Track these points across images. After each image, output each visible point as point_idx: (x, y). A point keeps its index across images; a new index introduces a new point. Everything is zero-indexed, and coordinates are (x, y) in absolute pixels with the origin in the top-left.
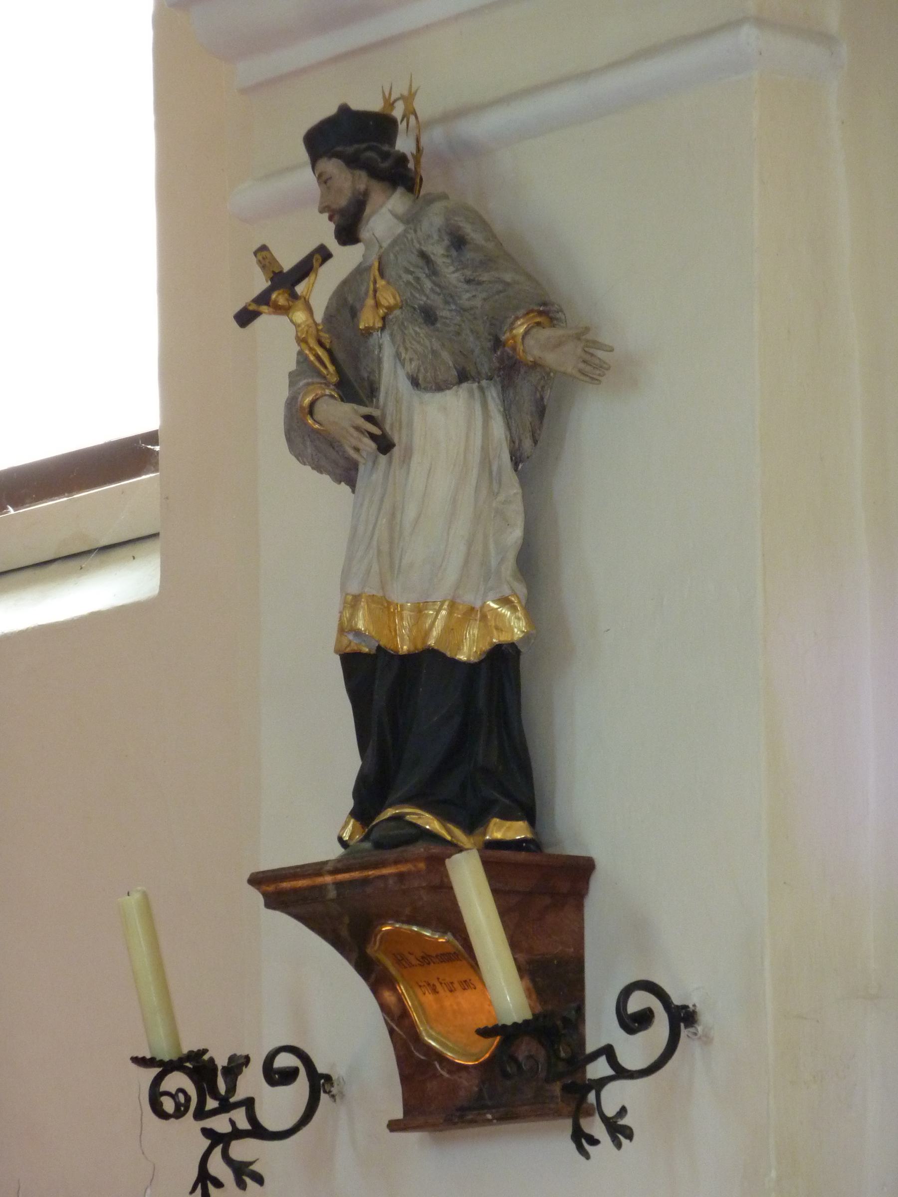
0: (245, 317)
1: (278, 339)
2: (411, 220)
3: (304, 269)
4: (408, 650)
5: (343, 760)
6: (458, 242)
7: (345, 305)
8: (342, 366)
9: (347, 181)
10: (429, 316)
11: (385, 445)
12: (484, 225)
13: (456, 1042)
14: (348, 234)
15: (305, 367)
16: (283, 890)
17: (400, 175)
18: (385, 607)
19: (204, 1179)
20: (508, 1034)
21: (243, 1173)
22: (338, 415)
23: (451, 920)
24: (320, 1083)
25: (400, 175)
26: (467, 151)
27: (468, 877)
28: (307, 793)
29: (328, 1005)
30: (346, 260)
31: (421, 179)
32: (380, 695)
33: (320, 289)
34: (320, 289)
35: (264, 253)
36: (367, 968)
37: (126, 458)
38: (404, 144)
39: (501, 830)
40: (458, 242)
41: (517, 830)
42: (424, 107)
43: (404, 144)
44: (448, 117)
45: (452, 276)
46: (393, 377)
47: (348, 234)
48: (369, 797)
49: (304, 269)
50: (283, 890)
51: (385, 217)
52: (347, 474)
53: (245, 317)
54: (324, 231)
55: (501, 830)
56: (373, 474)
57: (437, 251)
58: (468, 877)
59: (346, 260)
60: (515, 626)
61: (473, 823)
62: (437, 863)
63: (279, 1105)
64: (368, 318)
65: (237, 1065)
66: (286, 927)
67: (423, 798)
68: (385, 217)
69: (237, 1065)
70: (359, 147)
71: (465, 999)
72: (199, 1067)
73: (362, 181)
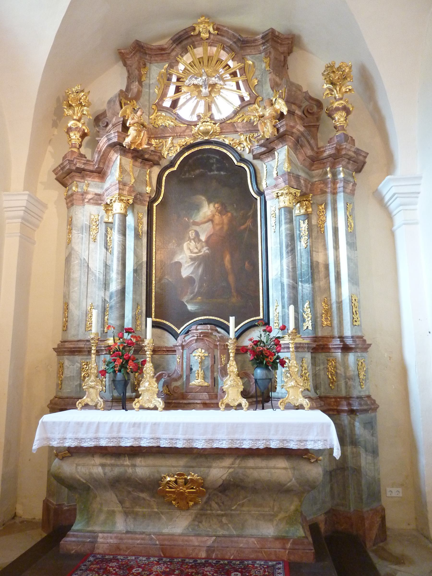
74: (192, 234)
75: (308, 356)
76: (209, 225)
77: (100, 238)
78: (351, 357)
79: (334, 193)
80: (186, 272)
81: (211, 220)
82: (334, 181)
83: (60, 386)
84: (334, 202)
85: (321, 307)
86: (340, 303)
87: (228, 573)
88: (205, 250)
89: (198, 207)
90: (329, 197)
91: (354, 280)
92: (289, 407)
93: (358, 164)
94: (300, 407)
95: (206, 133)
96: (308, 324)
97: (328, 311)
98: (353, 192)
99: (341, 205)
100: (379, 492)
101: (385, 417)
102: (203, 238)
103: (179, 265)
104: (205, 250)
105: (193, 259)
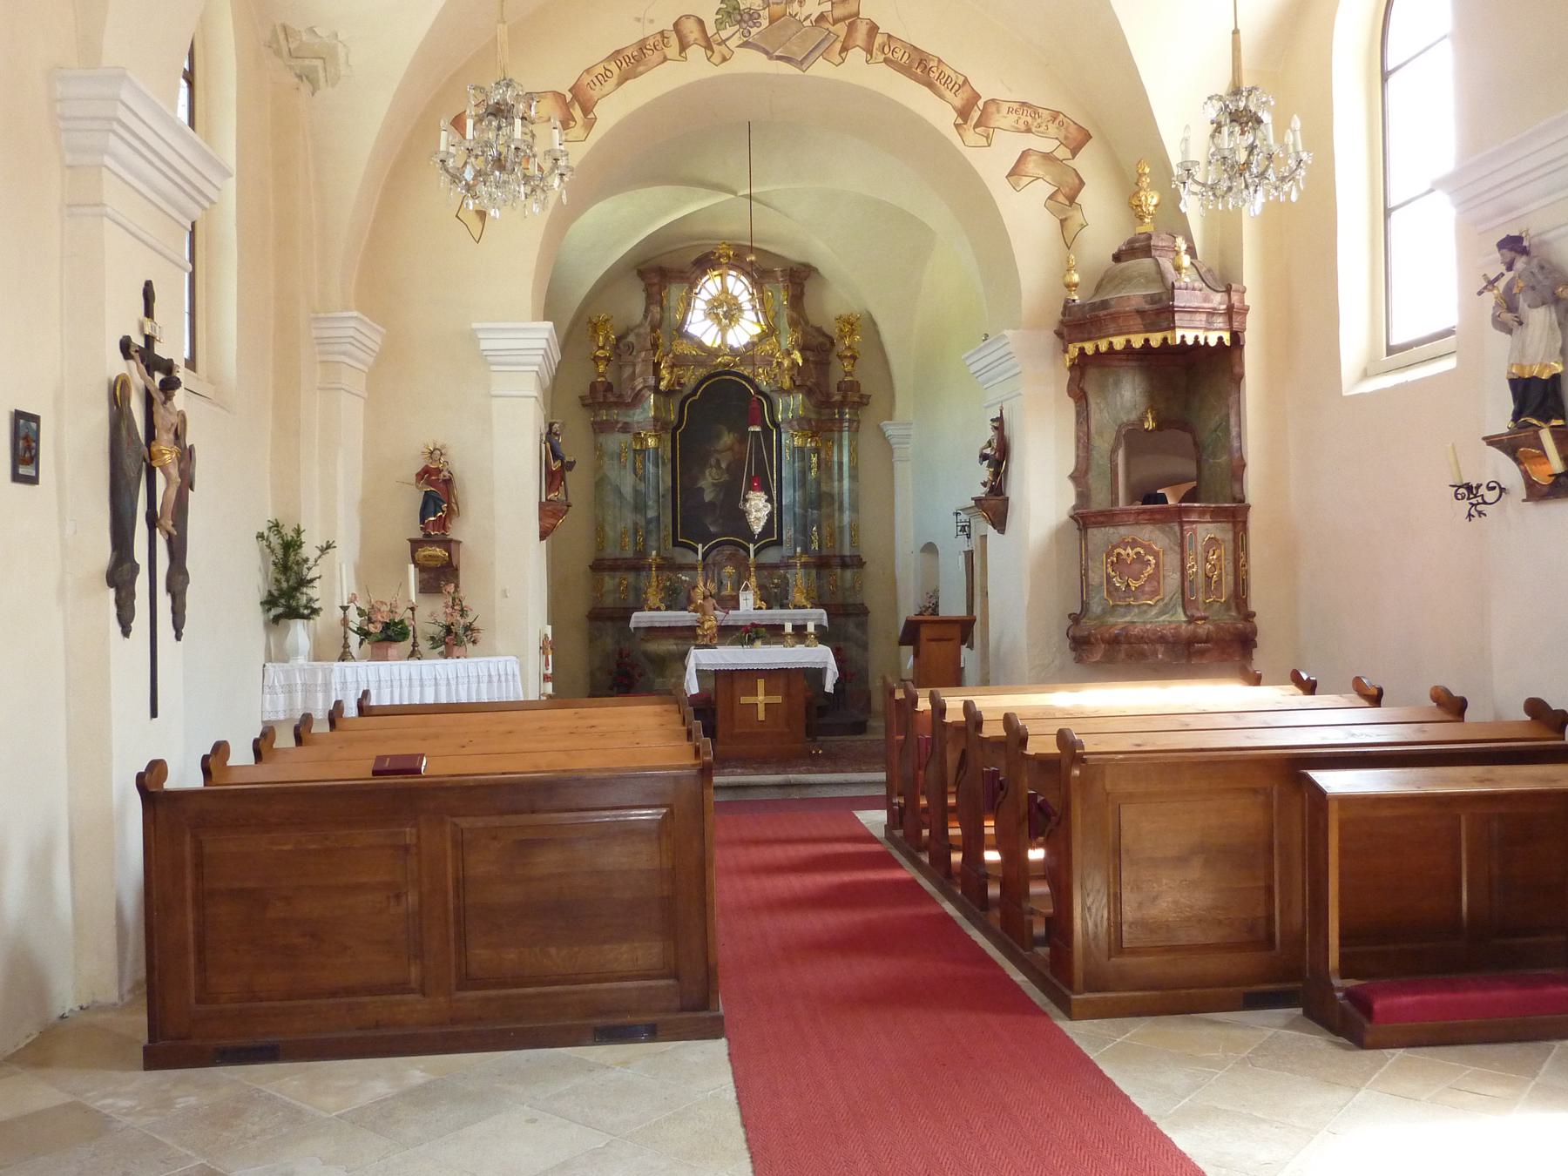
0: (1480, 293)
1: (1490, 298)
2: (1528, 263)
3: (1497, 279)
4: (1117, 384)
5: (1509, 406)
6: (1542, 268)
7: (1509, 287)
8: (1509, 303)
9: (1509, 255)
10: (1533, 288)
11: (1521, 323)
12: (1550, 263)
13: (1542, 475)
14: (1510, 268)
15: (1497, 305)
16: (1492, 441)
17: (1525, 251)
18: (1522, 367)
19: (1470, 515)
20: (1557, 476)
21: (1480, 513)
22: (1507, 317)
23: (1540, 447)
24: (1502, 490)
25: (1525, 251)
26: (1545, 243)
27: (1546, 437)
28: (1500, 414)
29: (1506, 470)
30: (1509, 275)
31: (186, 456)
32: (1520, 388)
33: (1502, 284)
34: (1502, 284)
35: (22, 470)
36: (1516, 460)
37: (1448, 333)
38: (1525, 243)
39: (1555, 423)
40: (1542, 268)
41: (1560, 422)
42: (1532, 233)
43: (1525, 243)
44: (1539, 235)
45: (1540, 277)
46: (1523, 305)
47: (1510, 268)
48: (1516, 416)
49: (1497, 279)
50: (1492, 441)
51: (1521, 263)
52: (1510, 332)
53: (1480, 293)
54: (1503, 268)
55: (1555, 423)
56: (1517, 331)
57: (1536, 270)
58: (1546, 437)
59: (1509, 275)
60: (1559, 369)
61: (1547, 421)
62: (1536, 432)
63: (1491, 496)
64: (1515, 290)
65: (1479, 486)
66: (1494, 452)
67: (1532, 415)
68: (1521, 263)
69: (1479, 486)
70: (1513, 245)
71: (1545, 467)
72: (1469, 487)
73: (1513, 254)
74: (713, 461)
75: (814, 572)
76: (729, 453)
77: (629, 465)
78: (848, 574)
79: (841, 431)
80: (708, 497)
81: (731, 449)
82: (841, 420)
83: (600, 547)
84: (841, 439)
85: (825, 531)
86: (841, 464)
87: (732, 13)
88: (726, 477)
89: (718, 437)
90: (836, 435)
91: (854, 477)
92: (796, 607)
93: (863, 402)
94: (804, 607)
95: (727, 365)
96: (815, 546)
97: (831, 535)
98: (857, 430)
99: (846, 443)
100: (866, 670)
101: (871, 568)
102: (724, 465)
103: (701, 490)
104: (726, 477)
105: (714, 485)
